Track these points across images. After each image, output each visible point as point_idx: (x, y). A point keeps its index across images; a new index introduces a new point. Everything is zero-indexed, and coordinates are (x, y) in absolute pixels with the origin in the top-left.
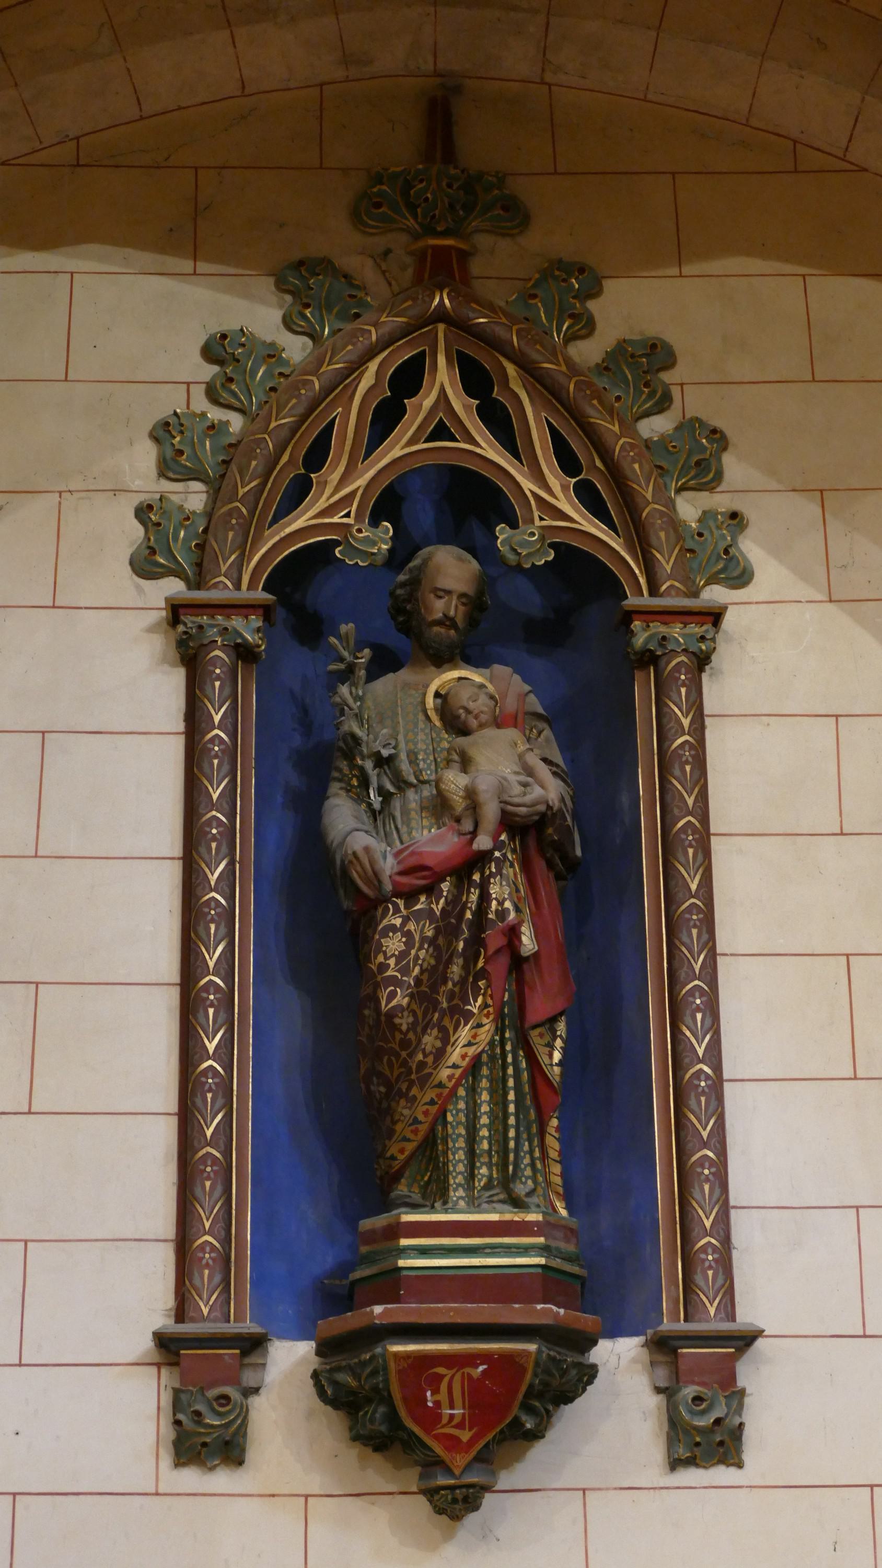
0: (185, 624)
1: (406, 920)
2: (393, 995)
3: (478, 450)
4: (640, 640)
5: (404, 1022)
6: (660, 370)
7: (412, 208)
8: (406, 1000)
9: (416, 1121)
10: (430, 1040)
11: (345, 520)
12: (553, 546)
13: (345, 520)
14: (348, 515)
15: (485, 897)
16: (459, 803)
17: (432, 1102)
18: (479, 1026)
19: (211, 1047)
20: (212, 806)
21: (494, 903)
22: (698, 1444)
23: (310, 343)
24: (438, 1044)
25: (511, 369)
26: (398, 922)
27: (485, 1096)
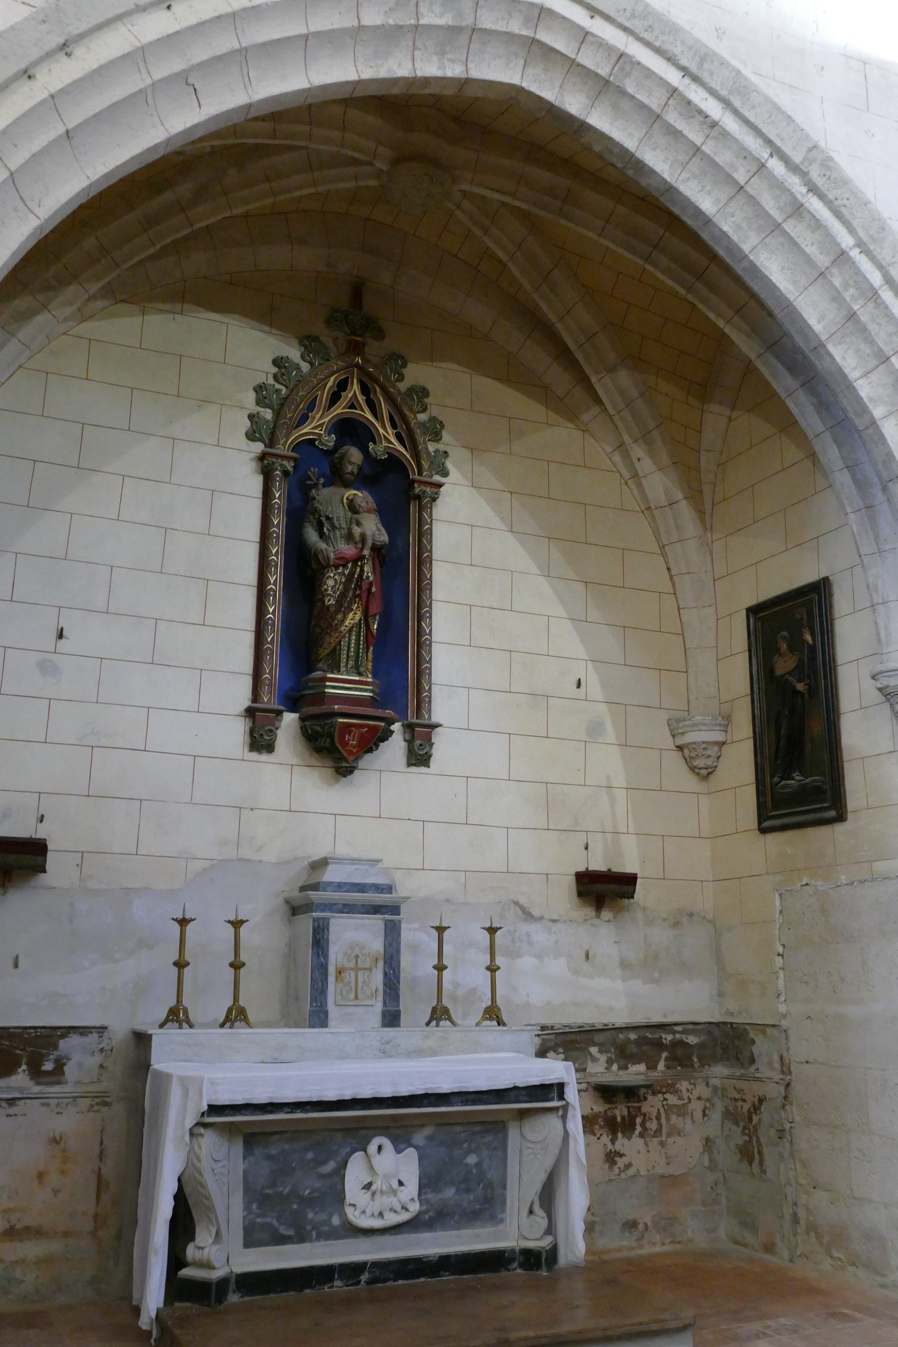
0: (268, 460)
1: (335, 575)
2: (329, 600)
3: (365, 415)
4: (417, 490)
5: (332, 610)
6: (425, 398)
7: (348, 324)
8: (334, 603)
9: (330, 643)
10: (340, 616)
11: (321, 432)
12: (388, 453)
13: (321, 432)
14: (321, 430)
15: (362, 571)
16: (357, 537)
17: (337, 637)
18: (356, 614)
19: (271, 610)
20: (274, 526)
21: (365, 573)
22: (418, 759)
23: (310, 366)
24: (343, 618)
25: (378, 389)
26: (332, 575)
27: (354, 637)
